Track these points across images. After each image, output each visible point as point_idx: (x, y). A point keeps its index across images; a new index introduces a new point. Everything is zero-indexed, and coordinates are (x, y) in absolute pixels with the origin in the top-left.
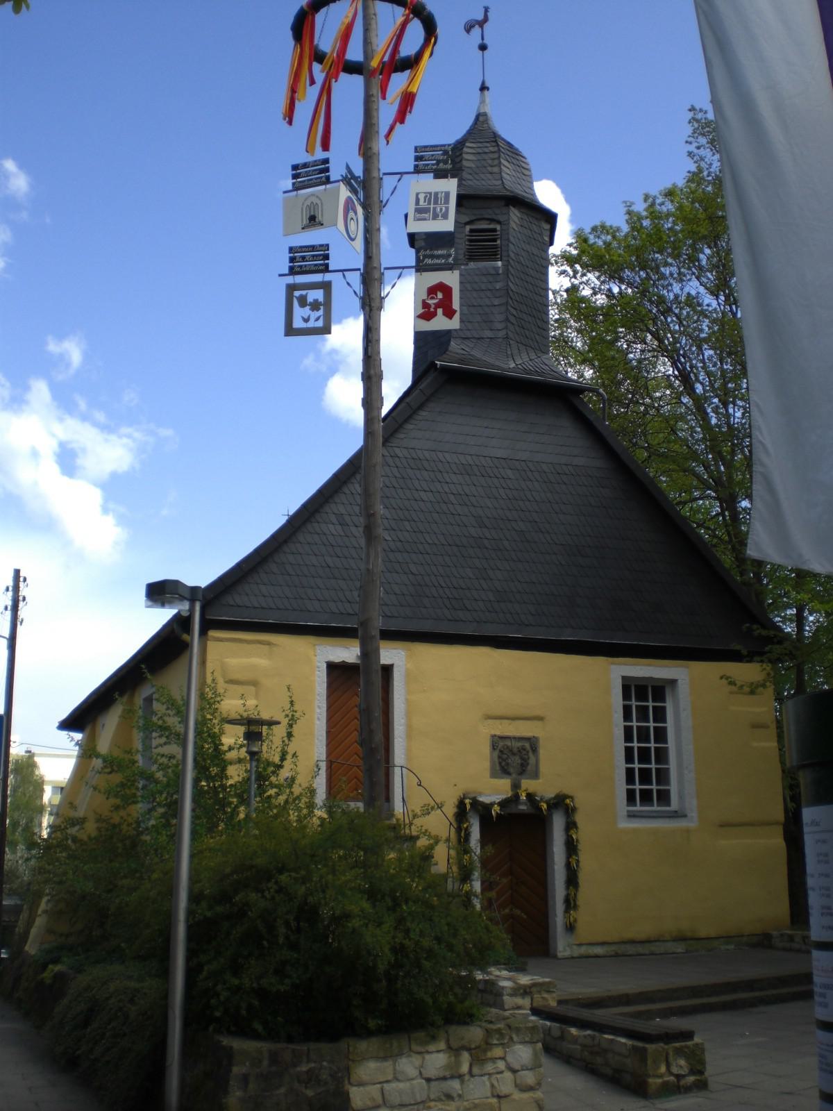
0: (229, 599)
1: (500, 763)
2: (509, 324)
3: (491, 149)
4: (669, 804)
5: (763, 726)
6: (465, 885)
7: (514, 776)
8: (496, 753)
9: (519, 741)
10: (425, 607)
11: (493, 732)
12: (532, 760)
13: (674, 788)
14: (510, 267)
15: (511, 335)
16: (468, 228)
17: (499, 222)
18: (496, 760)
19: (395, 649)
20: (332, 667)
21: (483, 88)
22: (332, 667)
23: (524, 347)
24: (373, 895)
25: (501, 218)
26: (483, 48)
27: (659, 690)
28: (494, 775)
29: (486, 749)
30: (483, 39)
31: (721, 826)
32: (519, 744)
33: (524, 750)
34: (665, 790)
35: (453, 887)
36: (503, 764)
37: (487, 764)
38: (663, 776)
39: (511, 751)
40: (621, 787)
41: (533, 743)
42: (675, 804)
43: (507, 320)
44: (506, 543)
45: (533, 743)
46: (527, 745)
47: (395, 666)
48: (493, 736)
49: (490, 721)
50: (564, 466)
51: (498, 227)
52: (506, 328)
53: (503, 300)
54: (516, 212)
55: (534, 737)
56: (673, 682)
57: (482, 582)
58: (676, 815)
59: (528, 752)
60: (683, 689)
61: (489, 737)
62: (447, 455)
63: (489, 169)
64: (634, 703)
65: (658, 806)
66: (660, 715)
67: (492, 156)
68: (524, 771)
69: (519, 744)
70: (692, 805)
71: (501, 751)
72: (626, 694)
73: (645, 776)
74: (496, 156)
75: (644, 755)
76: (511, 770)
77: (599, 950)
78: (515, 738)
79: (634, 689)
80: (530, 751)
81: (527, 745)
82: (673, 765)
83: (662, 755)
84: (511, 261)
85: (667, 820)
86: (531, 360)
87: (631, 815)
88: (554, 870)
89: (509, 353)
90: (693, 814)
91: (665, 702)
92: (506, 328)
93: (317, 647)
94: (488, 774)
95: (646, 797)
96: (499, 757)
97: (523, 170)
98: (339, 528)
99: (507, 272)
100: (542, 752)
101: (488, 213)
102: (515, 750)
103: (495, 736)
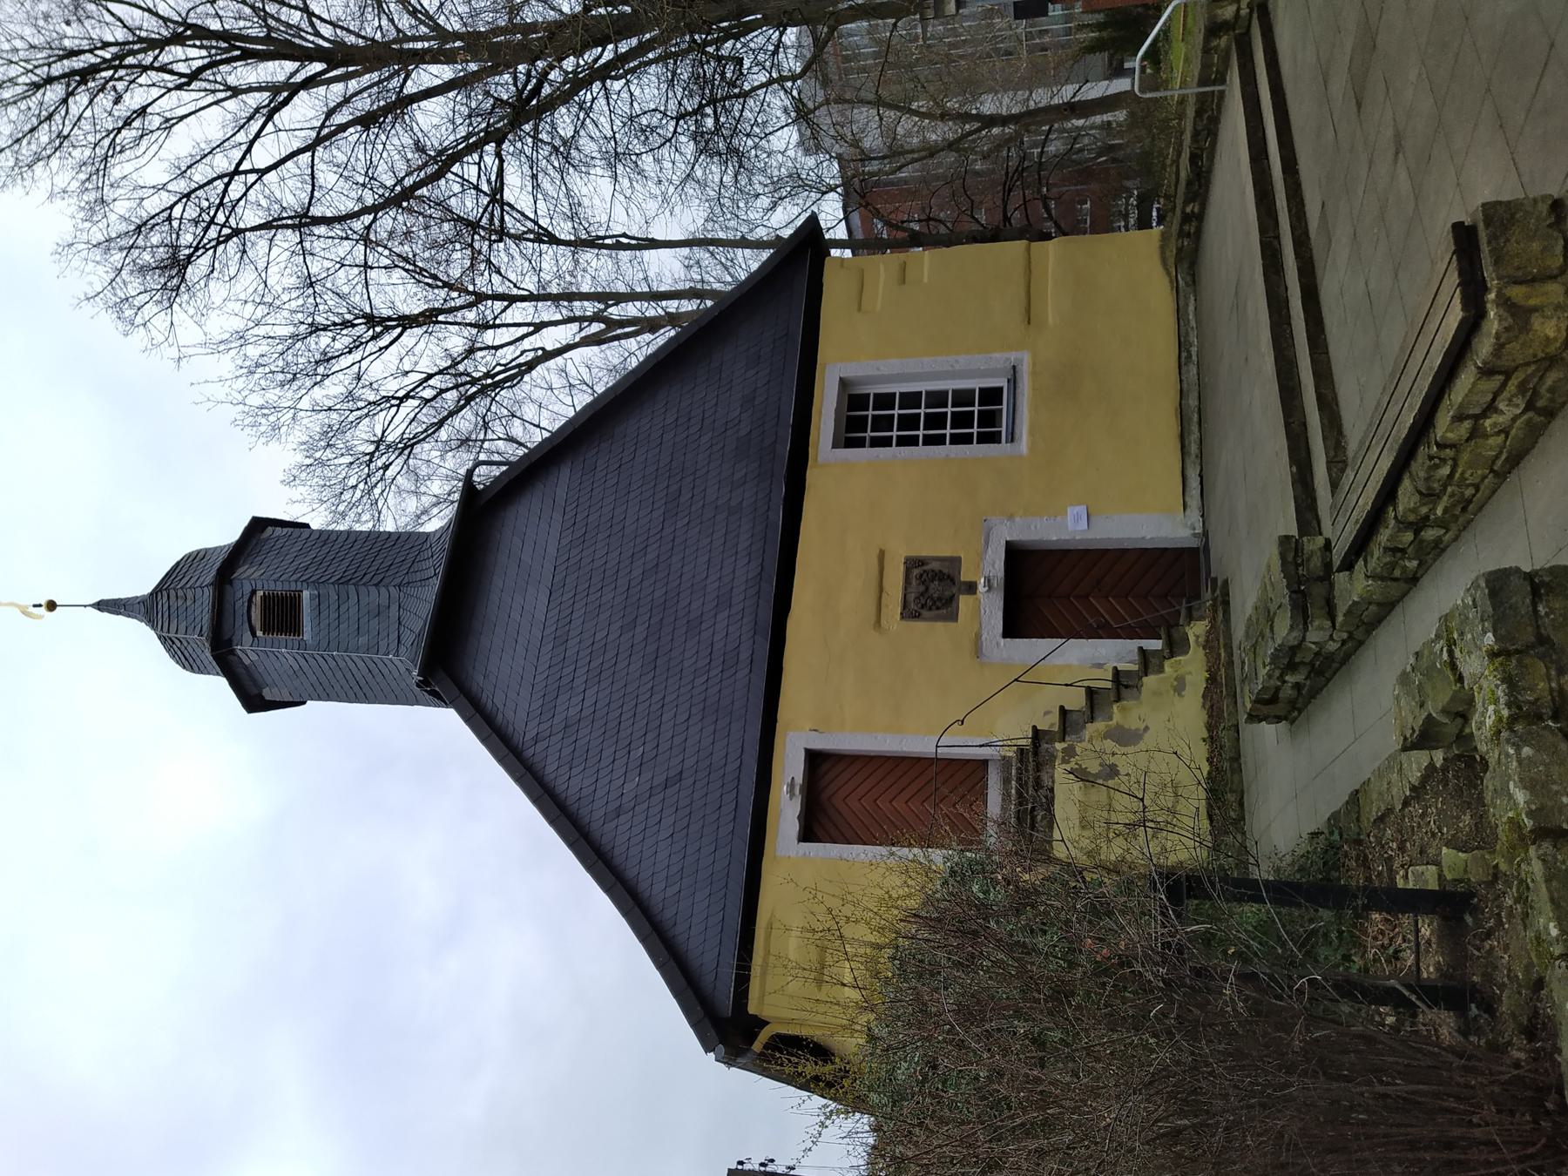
0: (707, 980)
1: (938, 608)
2: (383, 583)
3: (165, 599)
4: (1001, 389)
5: (903, 268)
6: (695, 308)
7: (954, 590)
8: (925, 613)
9: (911, 584)
10: (733, 703)
11: (898, 617)
12: (935, 566)
13: (976, 384)
14: (311, 580)
15: (397, 581)
16: (259, 633)
17: (254, 592)
18: (934, 613)
19: (784, 745)
20: (808, 833)
21: (52, 606)
22: (808, 833)
23: (416, 564)
24: (1018, 912)
25: (247, 589)
26: (52, 606)
27: (853, 400)
28: (953, 617)
29: (919, 626)
30: (40, 606)
31: (1029, 323)
32: (914, 582)
33: (921, 575)
34: (993, 412)
35: (194, 59)
36: (939, 604)
37: (940, 626)
38: (963, 397)
39: (922, 594)
40: (975, 450)
41: (913, 564)
42: (1001, 382)
43: (376, 585)
44: (657, 594)
45: (913, 564)
46: (916, 572)
47: (809, 747)
48: (903, 617)
49: (883, 622)
50: (566, 518)
51: (260, 593)
52: (387, 587)
53: (352, 588)
54: (241, 570)
55: (905, 563)
56: (844, 383)
57: (704, 626)
58: (1013, 381)
59: (925, 571)
60: (851, 370)
61: (904, 622)
62: (540, 669)
63: (189, 603)
64: (869, 434)
65: (1001, 404)
66: (885, 401)
67: (173, 598)
68: (949, 576)
69: (914, 582)
70: (1001, 358)
71: (922, 607)
72: (859, 443)
73: (962, 420)
74: (172, 593)
75: (936, 421)
76: (948, 593)
77: (1194, 483)
78: (906, 589)
79: (851, 433)
80: (925, 568)
81: (916, 572)
82: (949, 385)
83: (938, 398)
84: (304, 578)
85: (1018, 391)
86: (432, 556)
87: (1012, 438)
88: (1081, 541)
89: (419, 584)
90: (1013, 356)
91: (868, 395)
92: (387, 587)
93: (778, 854)
94: (951, 625)
95: (989, 419)
96: (930, 609)
97: (198, 559)
98: (623, 819)
99: (317, 584)
100: (924, 552)
101: (241, 606)
102: (922, 588)
103: (901, 614)
